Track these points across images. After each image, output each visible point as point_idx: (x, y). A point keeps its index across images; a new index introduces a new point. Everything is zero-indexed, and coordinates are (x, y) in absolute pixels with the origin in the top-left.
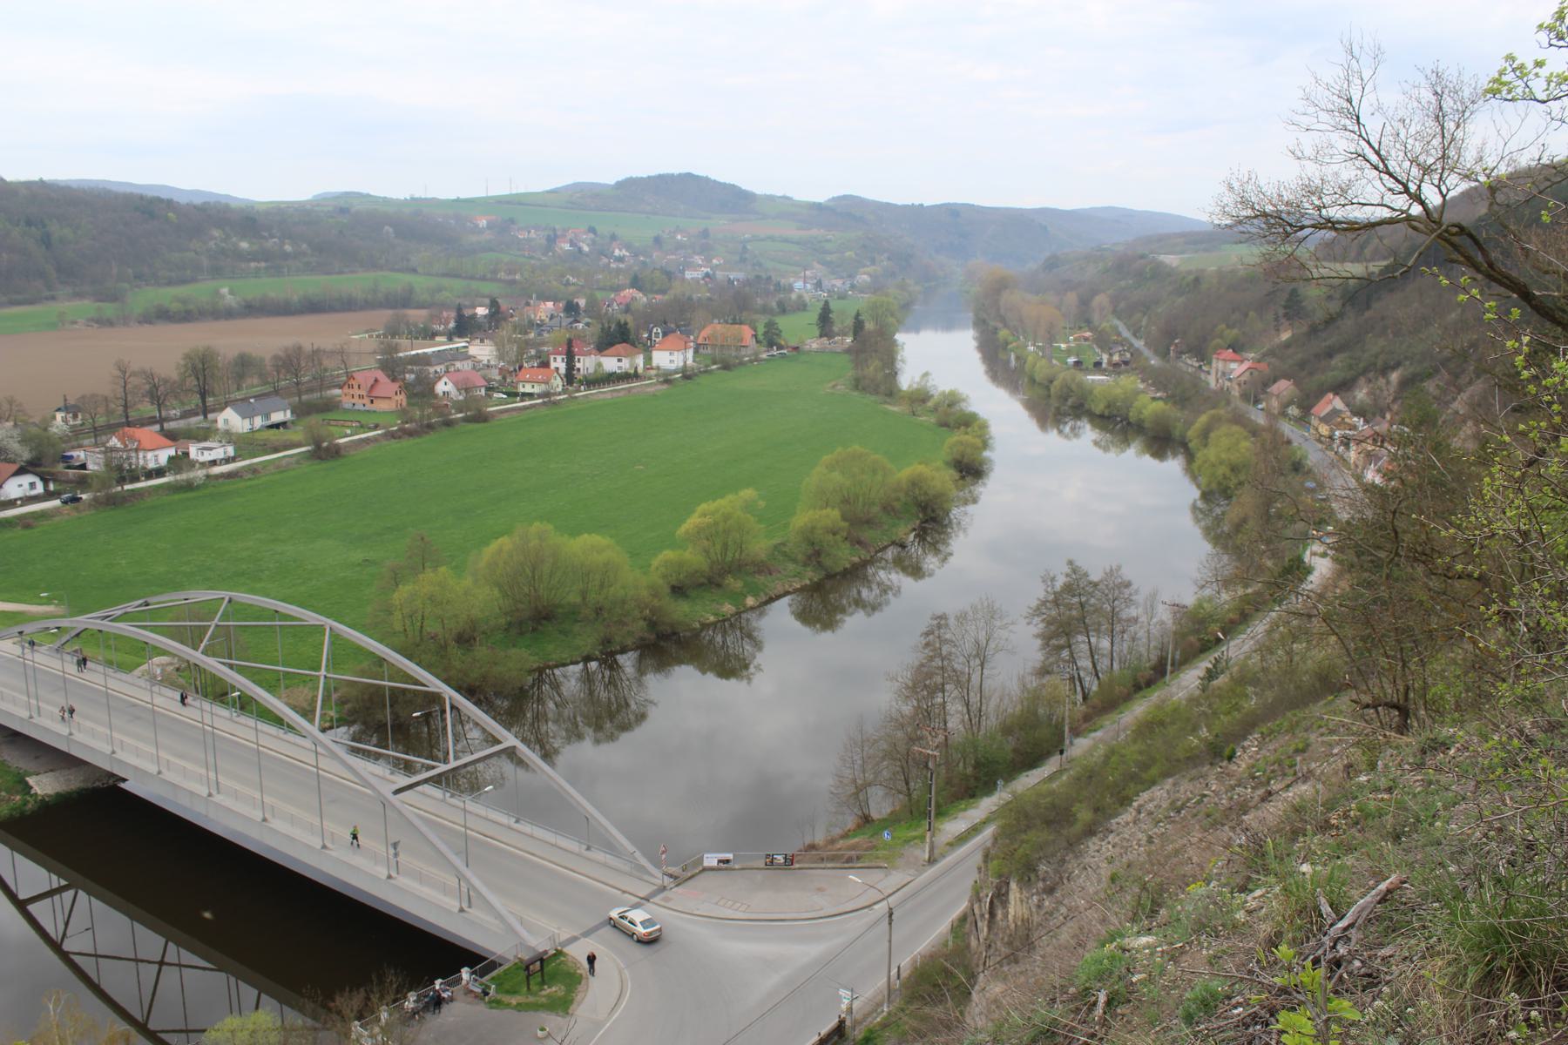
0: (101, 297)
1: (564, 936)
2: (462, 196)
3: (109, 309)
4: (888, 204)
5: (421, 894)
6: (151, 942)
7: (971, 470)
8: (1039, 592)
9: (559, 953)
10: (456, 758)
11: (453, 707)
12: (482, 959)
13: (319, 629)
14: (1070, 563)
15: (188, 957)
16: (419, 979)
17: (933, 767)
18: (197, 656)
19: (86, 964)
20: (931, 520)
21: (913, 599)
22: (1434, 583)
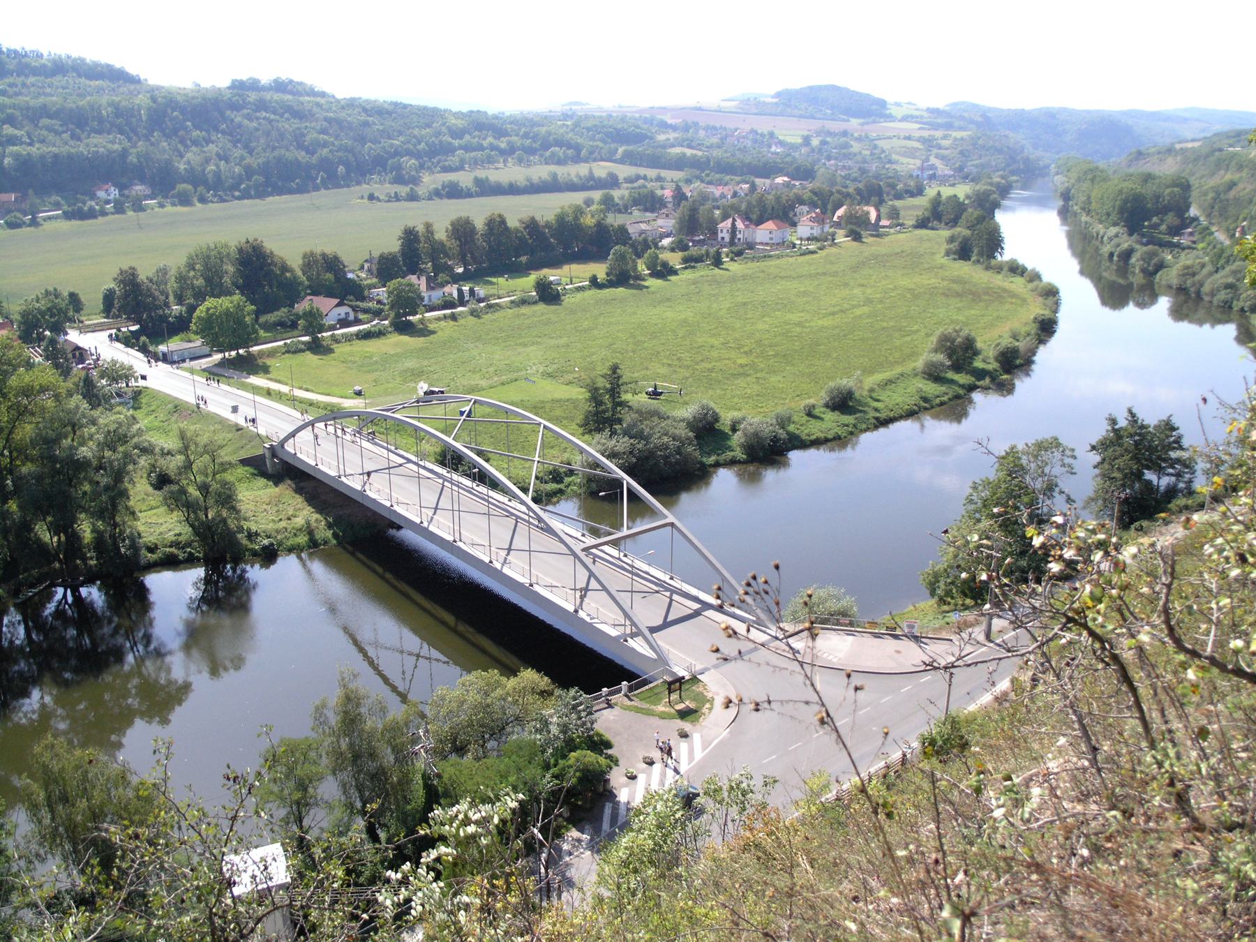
0: (399, 180)
1: (699, 667)
2: (656, 105)
3: (404, 190)
4: (591, 649)
5: (601, 620)
6: (412, 641)
7: (1046, 328)
8: (1100, 431)
9: (694, 679)
10: (628, 528)
11: (628, 490)
12: (637, 676)
13: (539, 424)
14: (1130, 411)
15: (435, 654)
16: (591, 687)
17: (1004, 558)
18: (450, 440)
19: (371, 652)
20: (1014, 363)
21: (999, 421)
22: (751, 897)
